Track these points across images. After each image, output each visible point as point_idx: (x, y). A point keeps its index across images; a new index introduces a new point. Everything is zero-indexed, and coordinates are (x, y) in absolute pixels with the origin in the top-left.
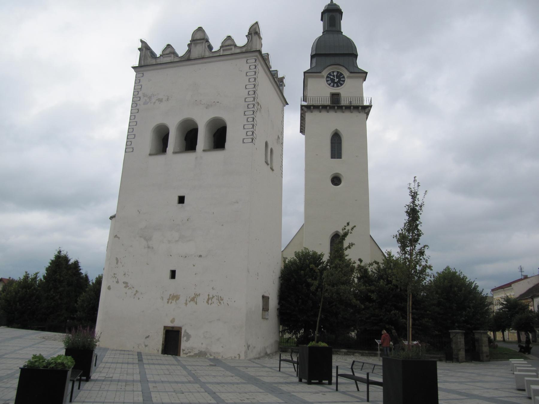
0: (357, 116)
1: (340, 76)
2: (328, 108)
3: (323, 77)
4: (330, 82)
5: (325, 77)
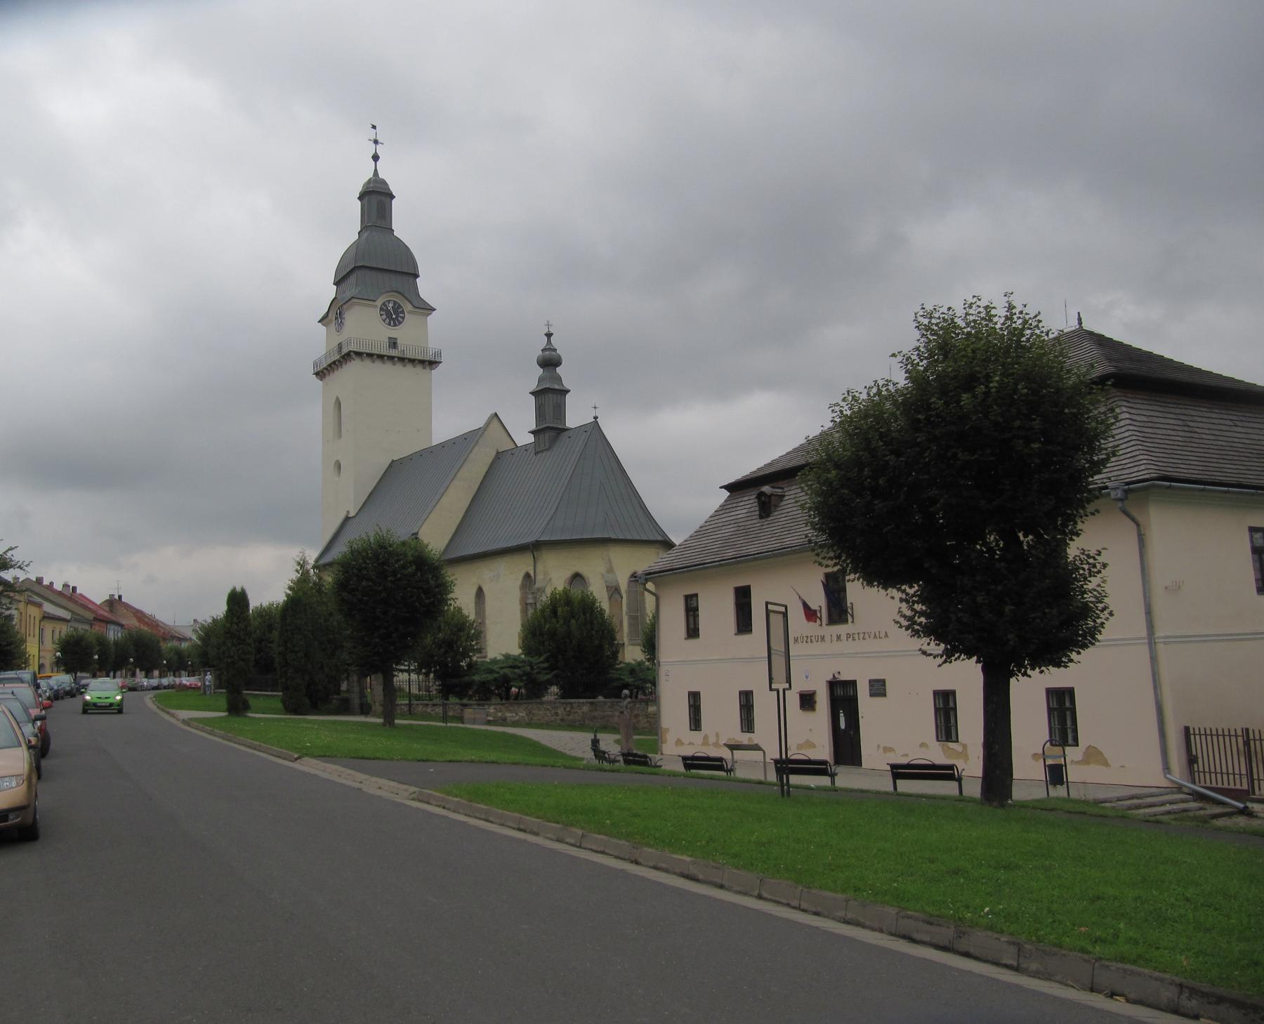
0: (418, 374)
1: (398, 309)
2: (386, 358)
3: (376, 306)
4: (384, 317)
5: (379, 307)
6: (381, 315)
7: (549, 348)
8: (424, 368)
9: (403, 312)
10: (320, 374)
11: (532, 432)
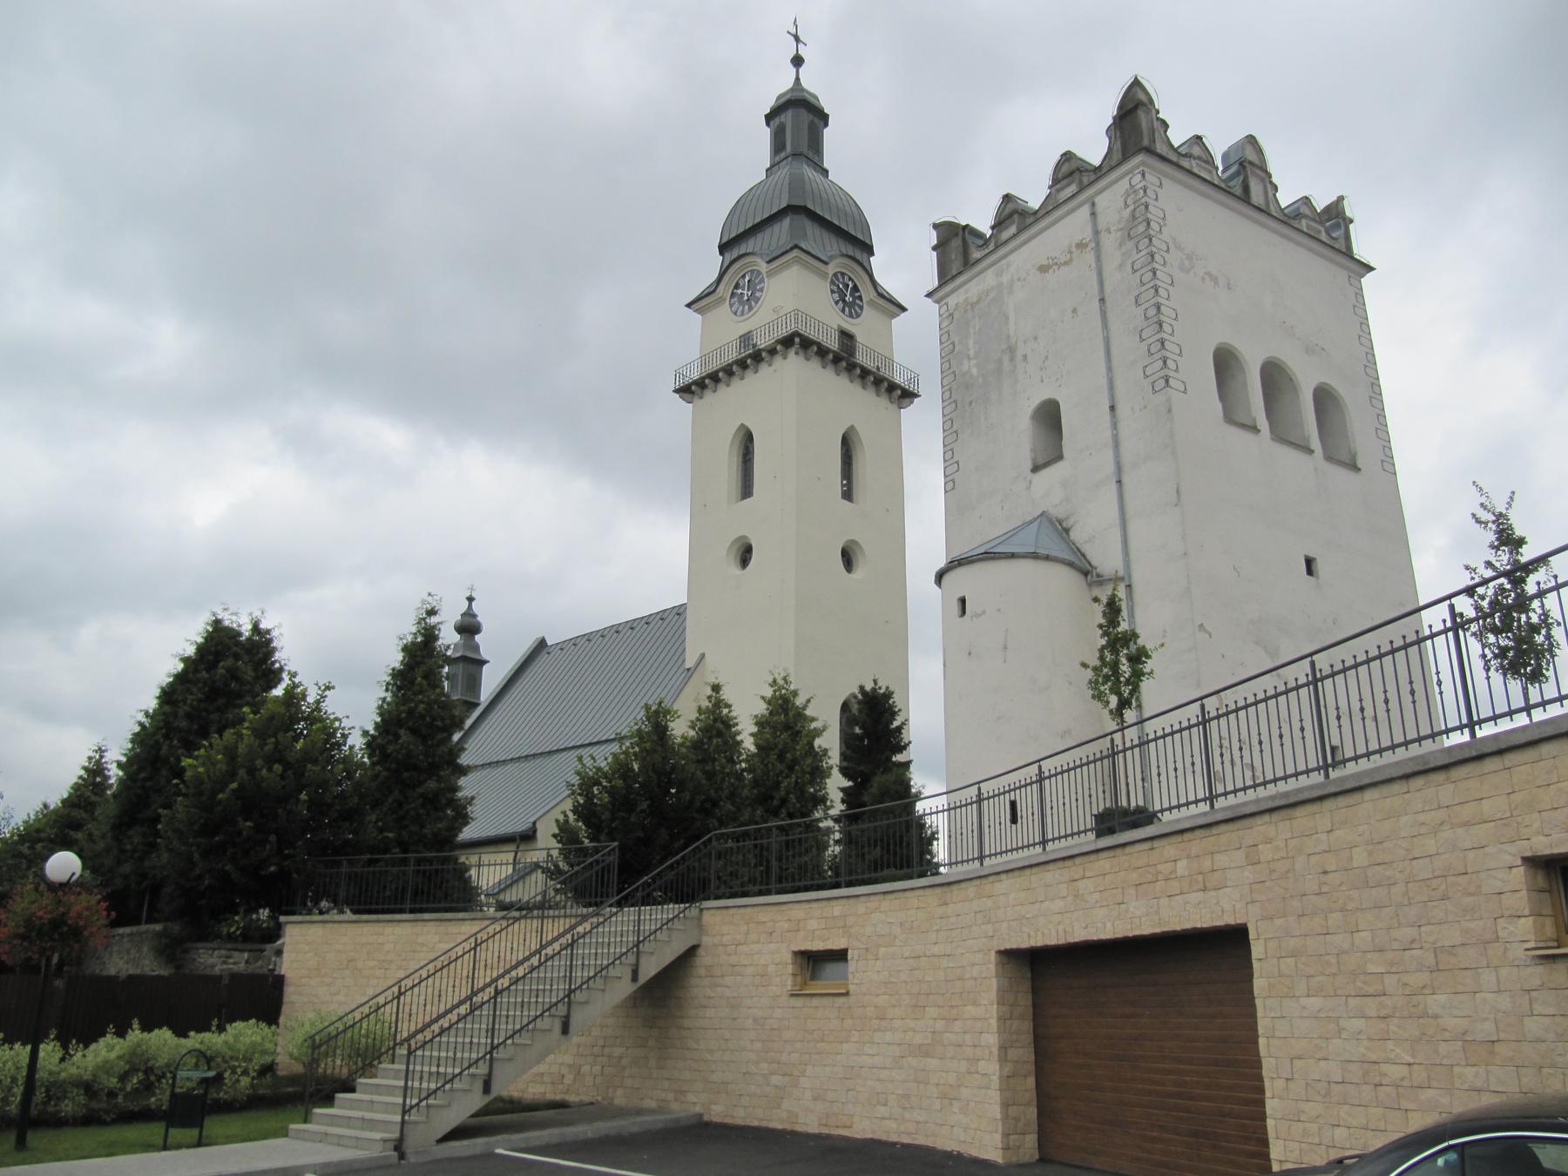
4: (836, 296)
7: (469, 614)
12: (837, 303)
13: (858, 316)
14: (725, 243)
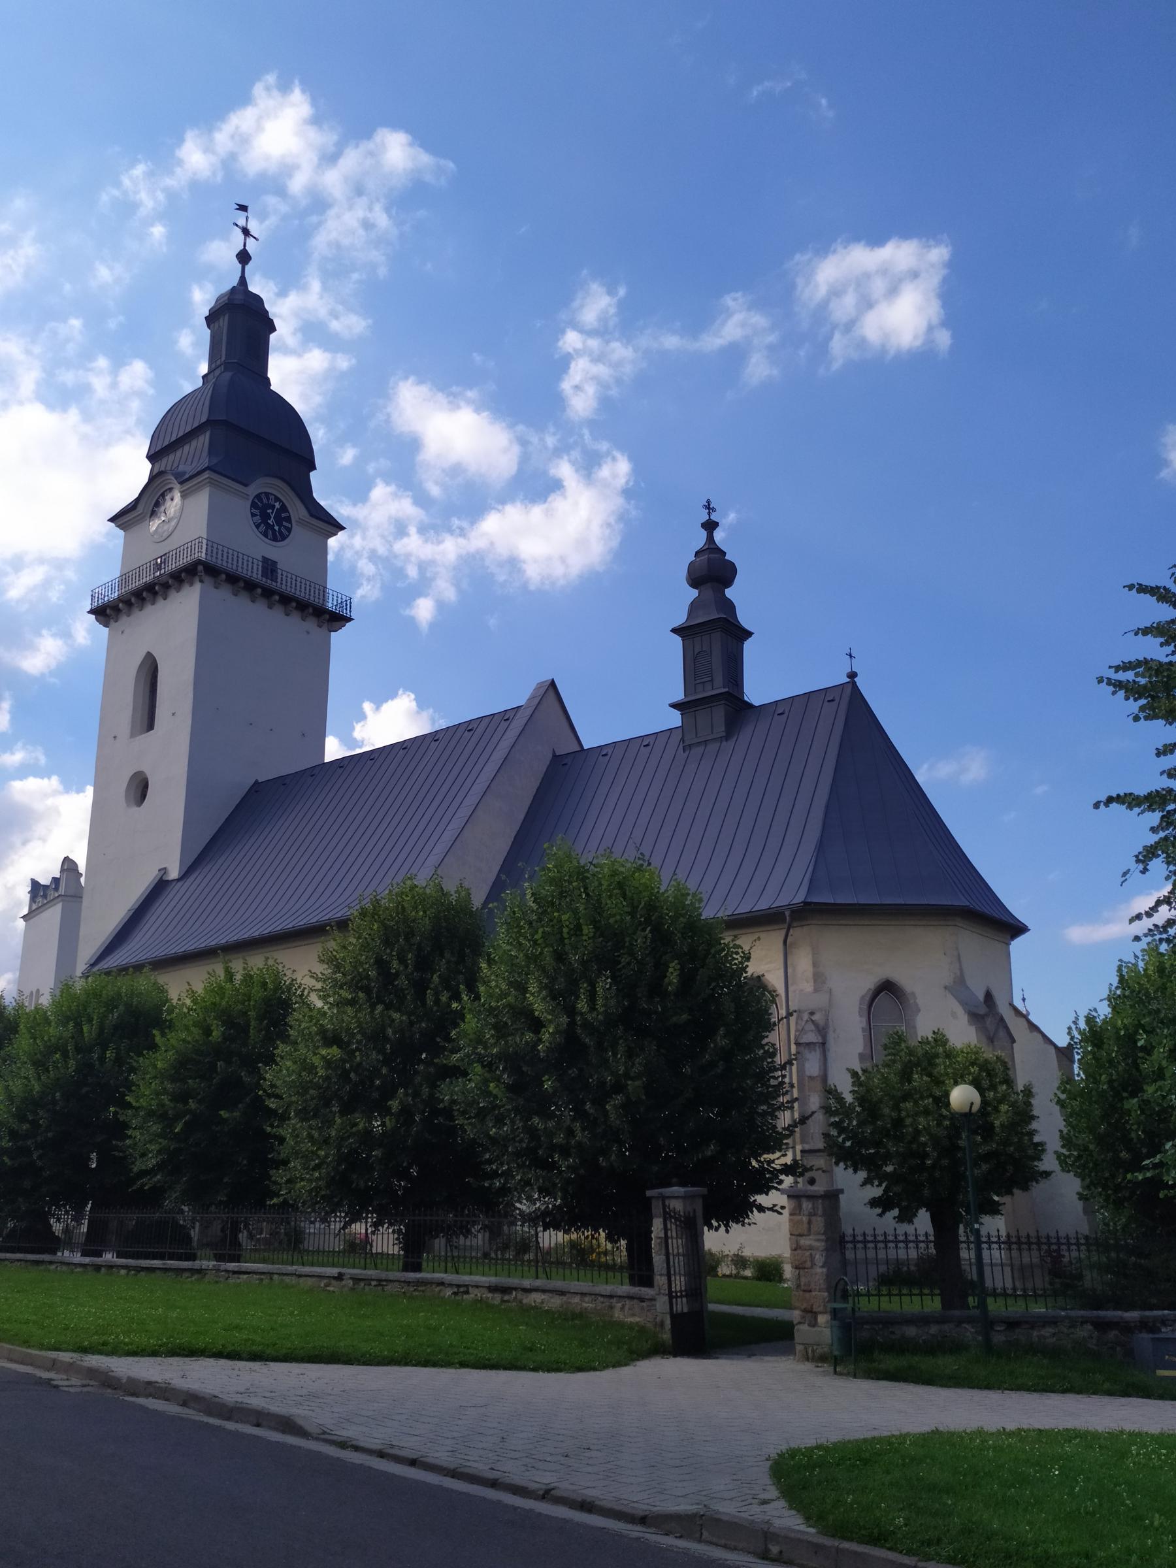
2: (259, 591)
4: (258, 519)
6: (253, 515)
7: (711, 550)
8: (320, 626)
9: (289, 519)
10: (104, 613)
11: (674, 706)
12: (258, 526)
13: (284, 538)
14: (159, 451)
